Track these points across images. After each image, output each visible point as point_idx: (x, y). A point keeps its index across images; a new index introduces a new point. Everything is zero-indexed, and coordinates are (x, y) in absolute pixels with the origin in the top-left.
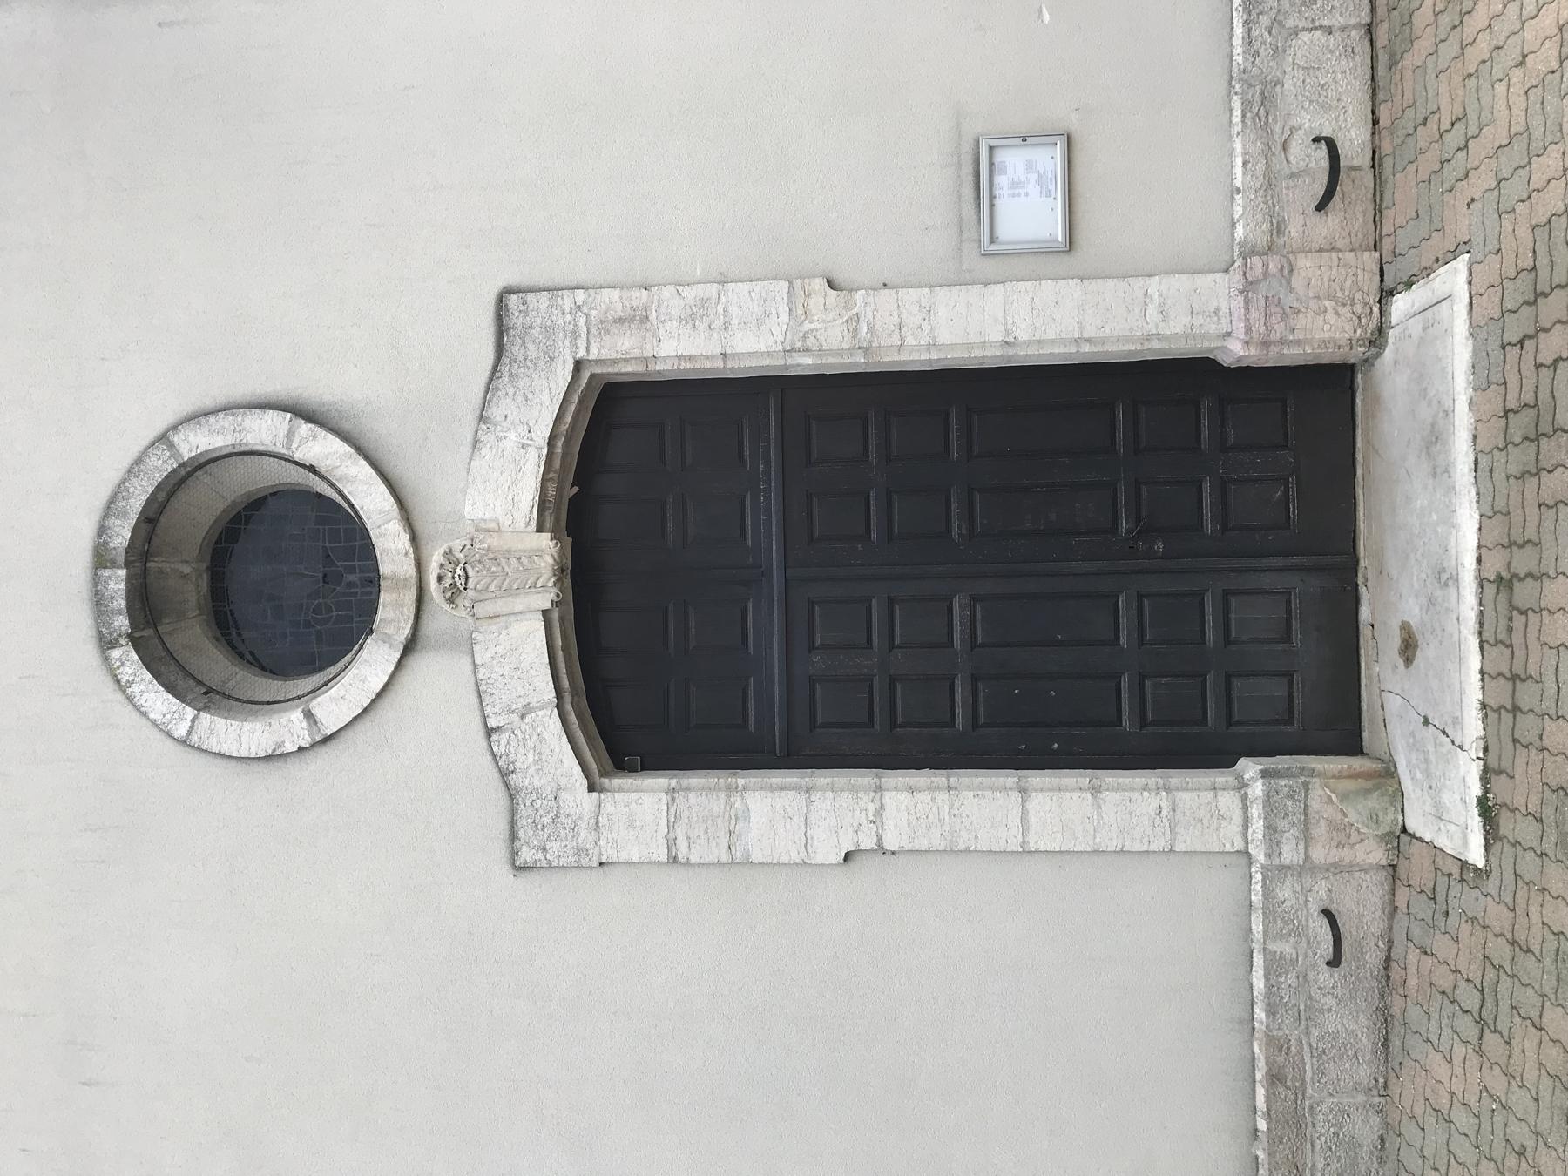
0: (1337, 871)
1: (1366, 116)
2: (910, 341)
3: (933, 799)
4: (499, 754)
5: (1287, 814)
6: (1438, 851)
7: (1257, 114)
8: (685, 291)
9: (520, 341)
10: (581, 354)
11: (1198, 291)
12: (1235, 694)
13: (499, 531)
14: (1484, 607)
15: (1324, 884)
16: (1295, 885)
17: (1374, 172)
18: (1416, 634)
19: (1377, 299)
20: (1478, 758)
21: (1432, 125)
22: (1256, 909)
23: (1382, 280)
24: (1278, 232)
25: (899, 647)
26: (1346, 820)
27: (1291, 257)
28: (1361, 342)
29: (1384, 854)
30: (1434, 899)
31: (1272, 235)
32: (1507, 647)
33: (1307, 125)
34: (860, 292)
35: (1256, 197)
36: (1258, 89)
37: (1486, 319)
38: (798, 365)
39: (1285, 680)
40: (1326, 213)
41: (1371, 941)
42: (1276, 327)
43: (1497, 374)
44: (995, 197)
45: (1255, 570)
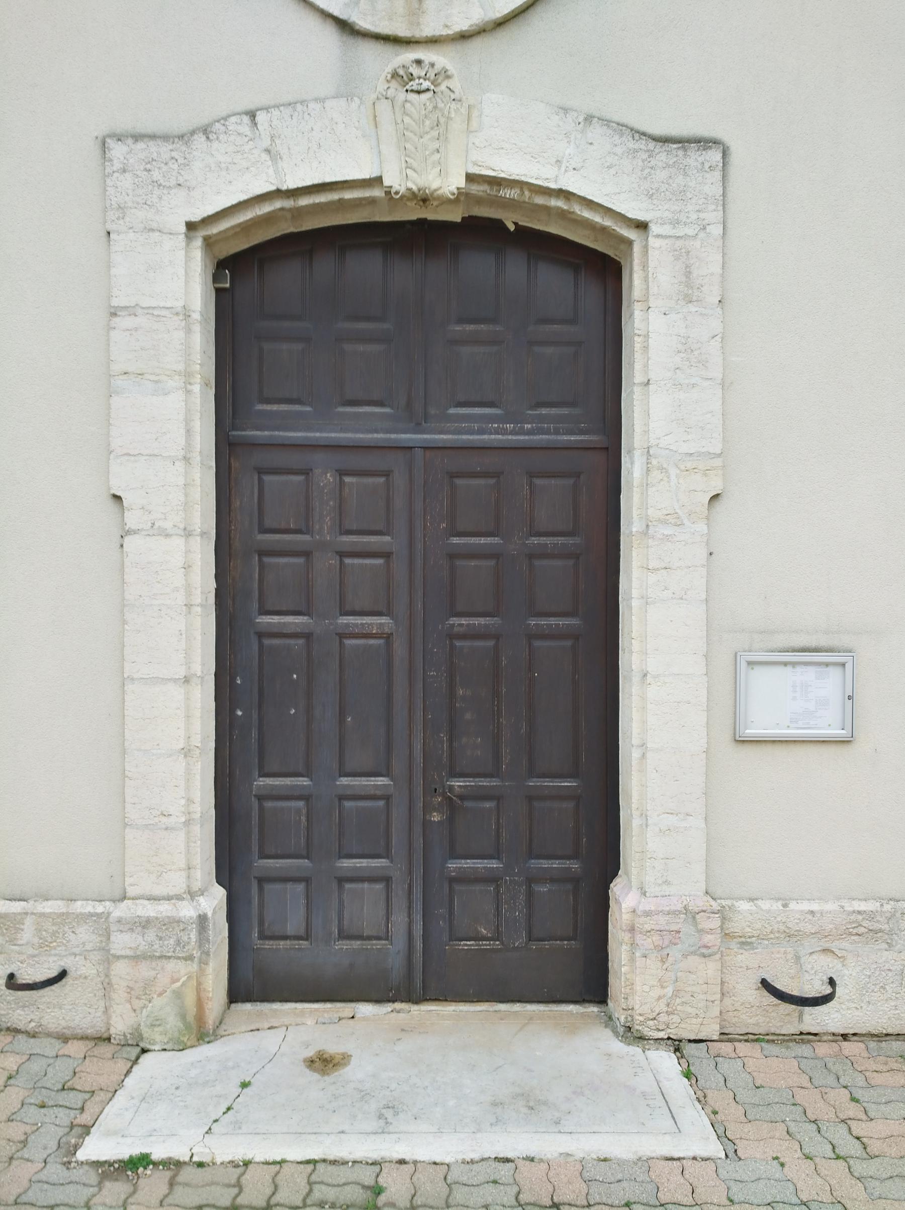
0: (105, 984)
1: (851, 1028)
2: (652, 578)
3: (177, 589)
4: (227, 123)
5: (161, 939)
6: (111, 1095)
7: (861, 925)
8: (716, 344)
9: (671, 163)
10: (654, 229)
11: (688, 865)
12: (289, 886)
13: (469, 131)
14: (353, 1166)
15: (92, 972)
16: (91, 944)
17: (796, 1035)
18: (336, 1074)
19: (672, 1036)
20: (192, 1154)
21: (852, 1110)
22: (68, 906)
23: (690, 1041)
24: (743, 943)
25: (341, 562)
26: (155, 996)
27: (718, 956)
28: (629, 1019)
29: (121, 1031)
30: (63, 1089)
31: (741, 937)
32: (304, 1200)
33: (846, 972)
34: (705, 527)
35: (778, 922)
36: (885, 927)
37: (657, 1180)
38: (632, 463)
39: (302, 932)
40: (758, 989)
41: (35, 1016)
42: (649, 940)
43: (599, 1194)
44: (794, 667)
45: (410, 908)
